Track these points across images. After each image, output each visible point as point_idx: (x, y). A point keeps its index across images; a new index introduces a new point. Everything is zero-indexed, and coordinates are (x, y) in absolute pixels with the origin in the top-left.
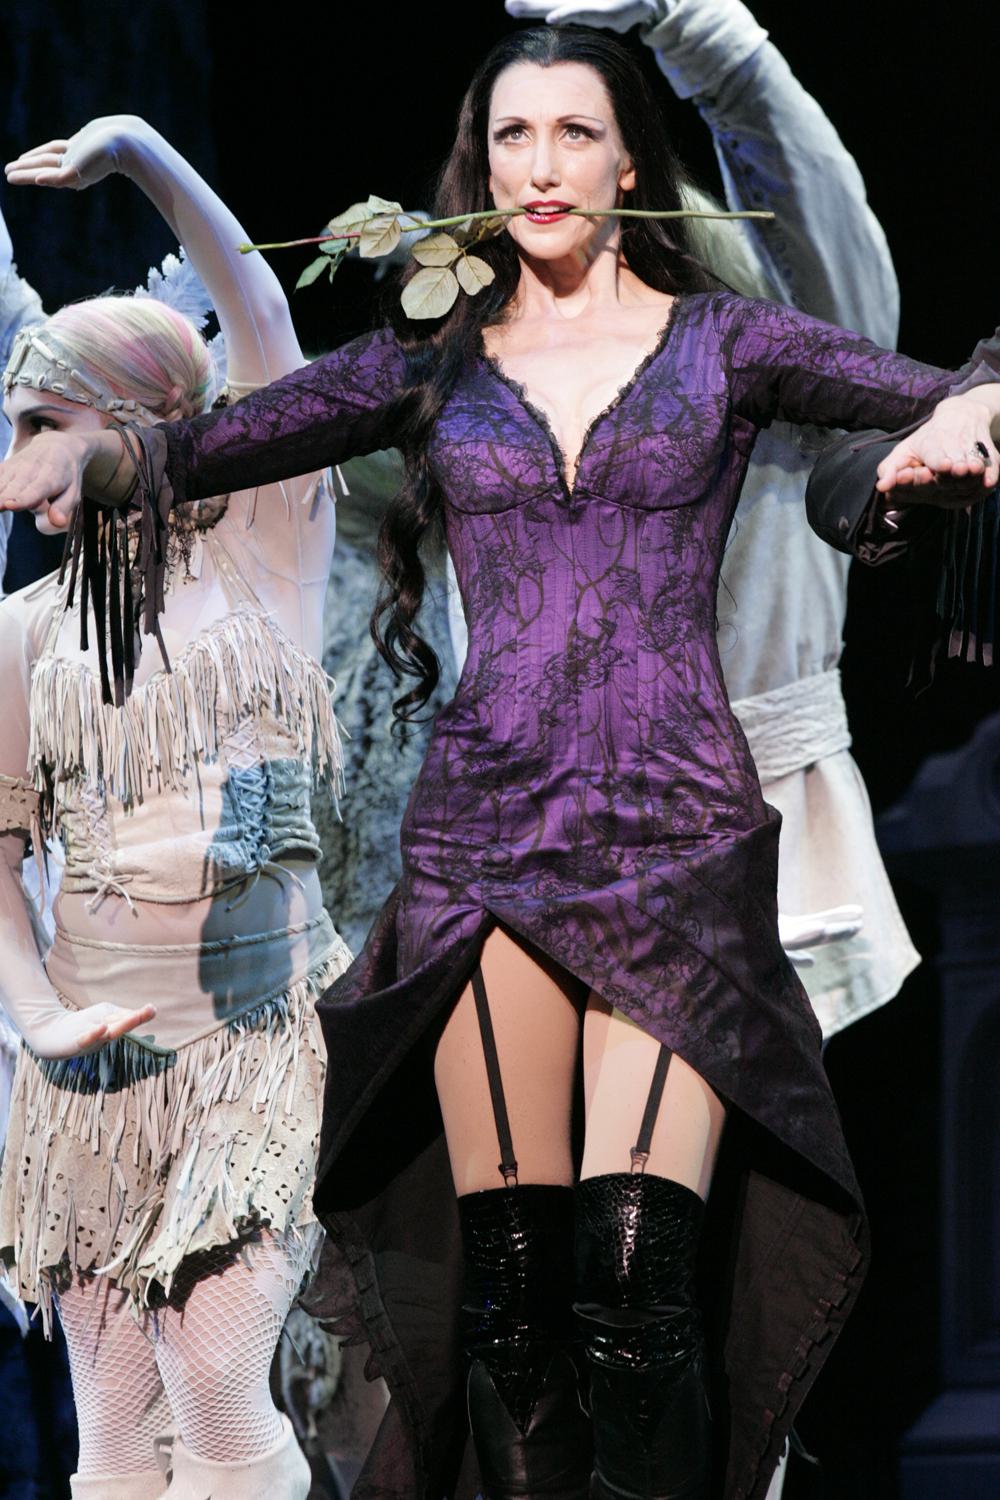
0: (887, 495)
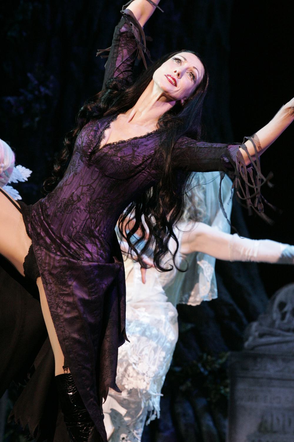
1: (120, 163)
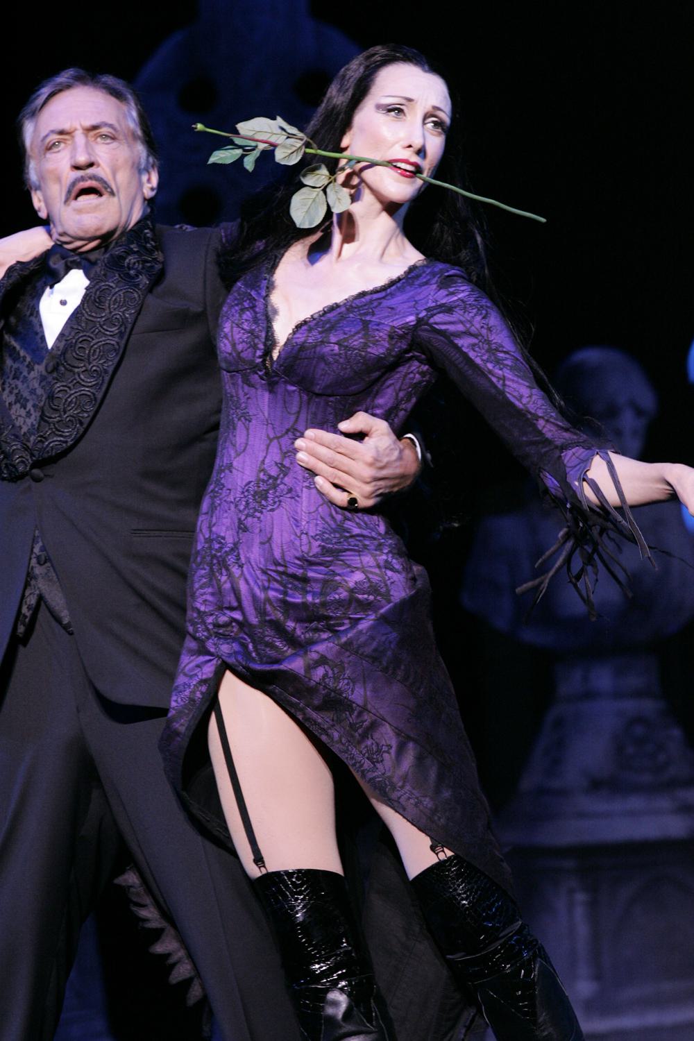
0: (535, 422)
1: (341, 358)
